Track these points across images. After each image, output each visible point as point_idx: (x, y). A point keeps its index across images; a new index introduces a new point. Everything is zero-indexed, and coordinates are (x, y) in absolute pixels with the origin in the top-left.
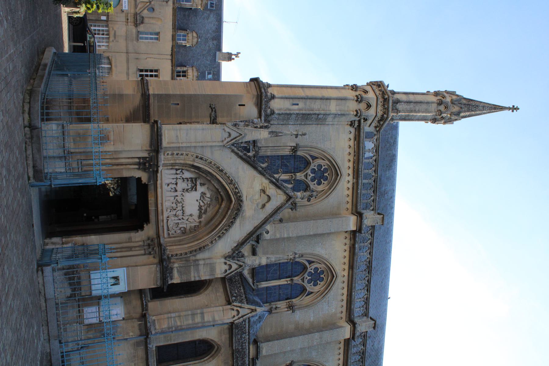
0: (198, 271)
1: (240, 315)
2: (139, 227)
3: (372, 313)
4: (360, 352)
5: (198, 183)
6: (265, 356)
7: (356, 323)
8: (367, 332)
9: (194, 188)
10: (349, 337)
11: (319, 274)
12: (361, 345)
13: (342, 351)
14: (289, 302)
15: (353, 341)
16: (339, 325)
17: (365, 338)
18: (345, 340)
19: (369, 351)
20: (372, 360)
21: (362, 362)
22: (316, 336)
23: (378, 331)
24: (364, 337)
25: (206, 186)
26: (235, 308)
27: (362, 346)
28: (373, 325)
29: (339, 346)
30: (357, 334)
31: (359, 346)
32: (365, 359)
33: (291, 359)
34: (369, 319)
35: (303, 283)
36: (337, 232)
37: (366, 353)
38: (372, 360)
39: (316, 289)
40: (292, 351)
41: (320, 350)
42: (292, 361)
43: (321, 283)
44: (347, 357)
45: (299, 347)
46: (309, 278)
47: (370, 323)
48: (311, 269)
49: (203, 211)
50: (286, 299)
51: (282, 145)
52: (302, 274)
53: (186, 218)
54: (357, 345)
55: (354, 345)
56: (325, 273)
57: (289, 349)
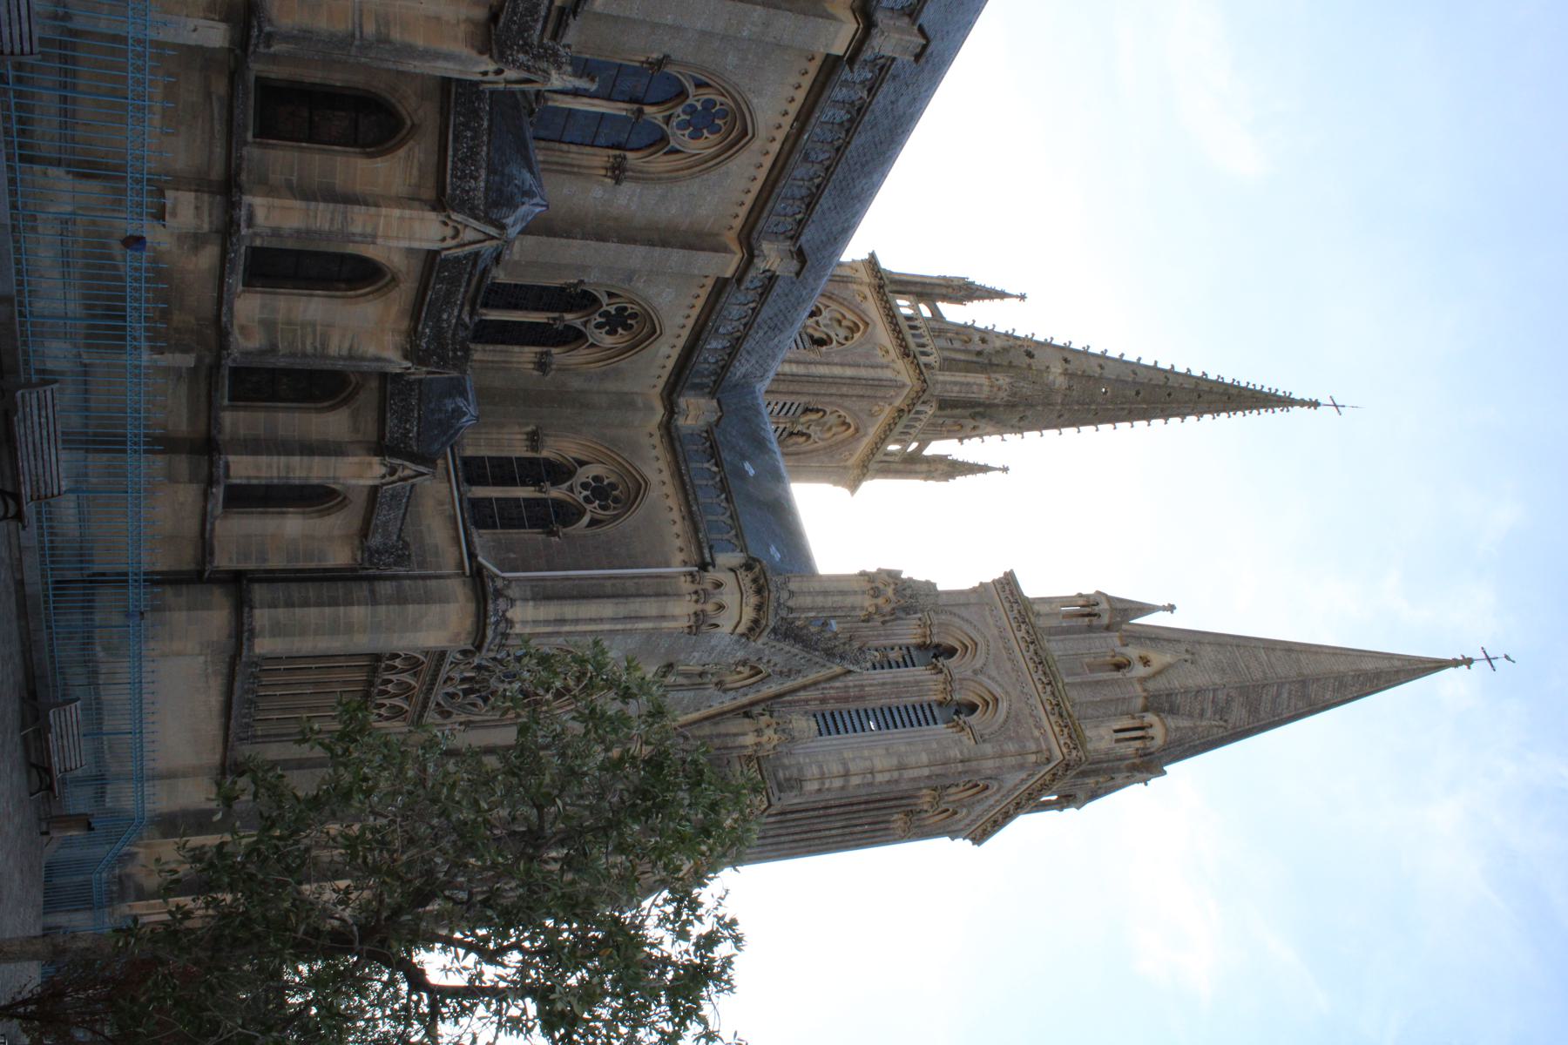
3: (928, 16)
4: (852, 103)
6: (599, 16)
7: (876, 26)
8: (894, 59)
10: (841, 53)
11: (714, 116)
12: (864, 87)
13: (807, 82)
14: (615, 157)
15: (847, 68)
16: (831, 10)
17: (883, 73)
18: (828, 55)
19: (878, 114)
20: (874, 137)
21: (848, 131)
22: (755, 15)
23: (923, 70)
24: (881, 69)
27: (866, 93)
28: (918, 50)
29: (805, 64)
30: (867, 54)
31: (857, 86)
32: (858, 126)
33: (666, 50)
34: (916, 28)
35: (665, 127)
37: (868, 114)
38: (874, 137)
39: (694, 147)
40: (677, 29)
41: (750, 56)
42: (666, 57)
43: (711, 137)
44: (815, 102)
45: (699, 26)
46: (683, 117)
47: (913, 38)
48: (696, 98)
50: (612, 147)
52: (670, 105)
54: (854, 82)
55: (846, 80)
57: (669, 19)
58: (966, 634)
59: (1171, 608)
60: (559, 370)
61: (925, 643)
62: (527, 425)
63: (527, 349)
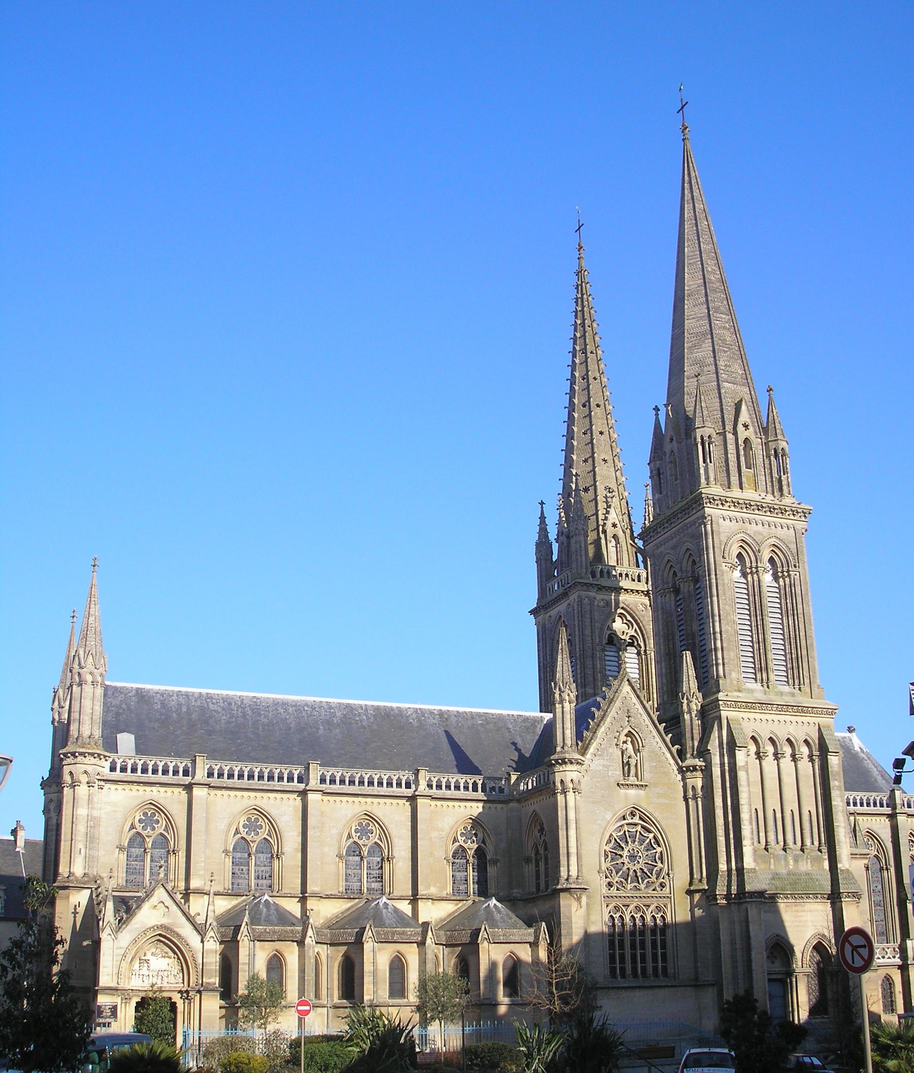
0: (211, 963)
1: (248, 935)
2: (173, 1007)
5: (144, 958)
9: (147, 961)
25: (147, 952)
26: (243, 938)
36: (207, 810)
49: (166, 955)
51: (117, 863)
53: (170, 969)
56: (250, 816)
58: (665, 568)
59: (657, 409)
60: (496, 855)
61: (673, 591)
62: (522, 865)
63: (488, 870)
